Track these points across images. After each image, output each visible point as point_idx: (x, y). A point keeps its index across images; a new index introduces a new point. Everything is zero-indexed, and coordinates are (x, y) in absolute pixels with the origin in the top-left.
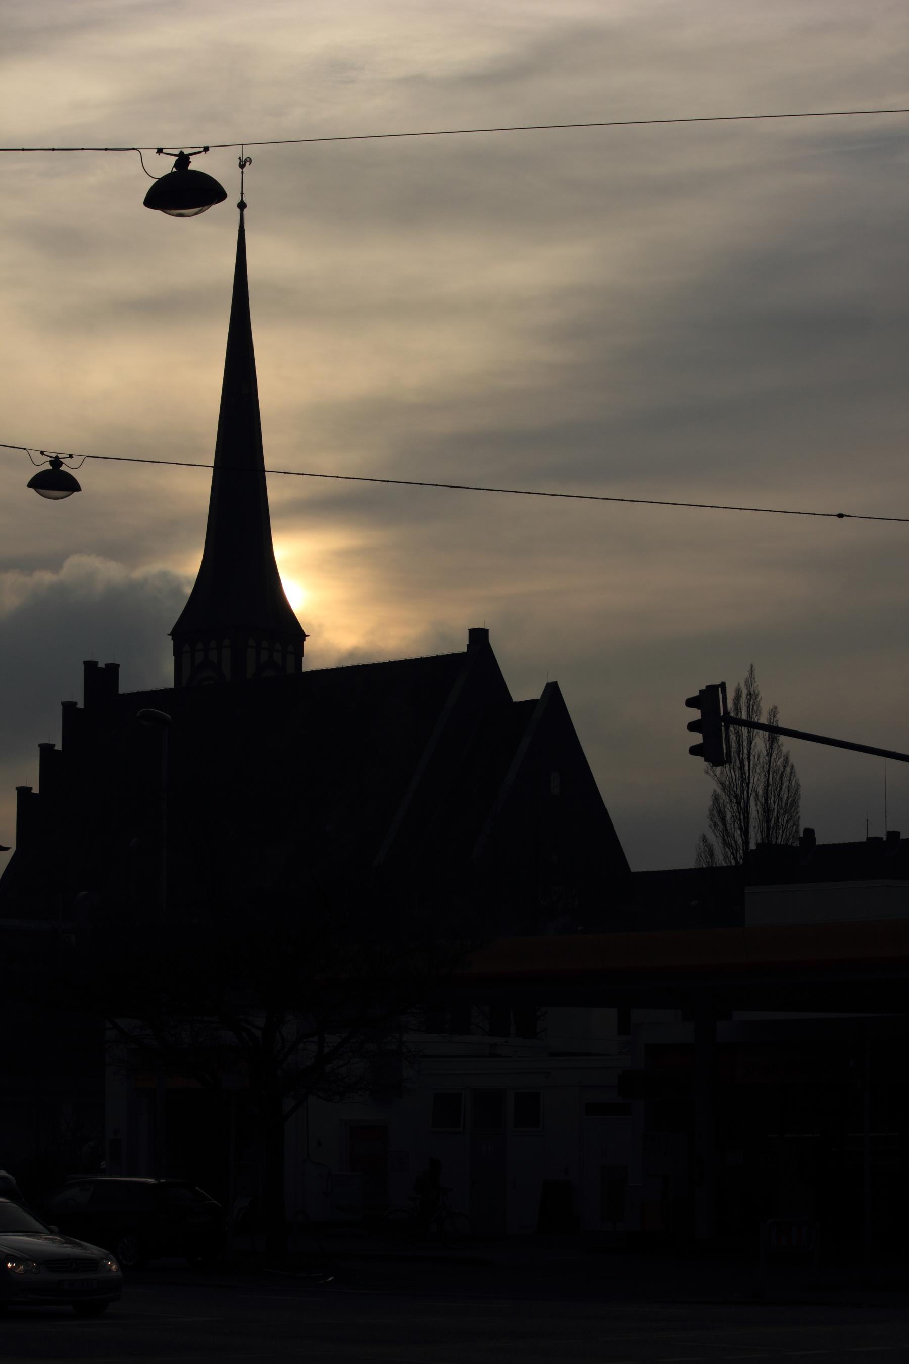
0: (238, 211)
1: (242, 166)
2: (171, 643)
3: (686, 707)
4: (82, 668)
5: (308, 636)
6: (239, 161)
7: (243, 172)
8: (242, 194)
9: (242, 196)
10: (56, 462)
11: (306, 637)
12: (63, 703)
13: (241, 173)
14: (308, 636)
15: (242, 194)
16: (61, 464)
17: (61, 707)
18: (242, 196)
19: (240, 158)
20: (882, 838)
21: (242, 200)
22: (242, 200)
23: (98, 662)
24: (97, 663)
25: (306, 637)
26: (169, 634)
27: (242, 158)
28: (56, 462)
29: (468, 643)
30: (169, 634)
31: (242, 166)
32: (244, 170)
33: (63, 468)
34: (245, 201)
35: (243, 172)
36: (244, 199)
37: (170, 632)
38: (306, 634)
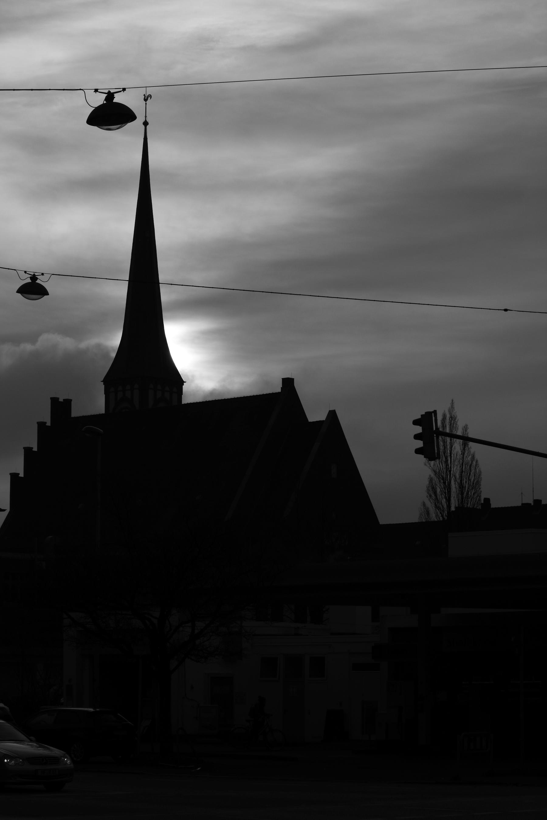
0: (143, 127)
2: (103, 387)
5: (185, 382)
7: (146, 104)
8: (146, 116)
9: (146, 118)
11: (184, 383)
14: (185, 382)
15: (146, 116)
18: (146, 118)
20: (531, 504)
25: (184, 383)
34: (147, 121)
35: (146, 104)
37: (102, 380)
38: (184, 381)
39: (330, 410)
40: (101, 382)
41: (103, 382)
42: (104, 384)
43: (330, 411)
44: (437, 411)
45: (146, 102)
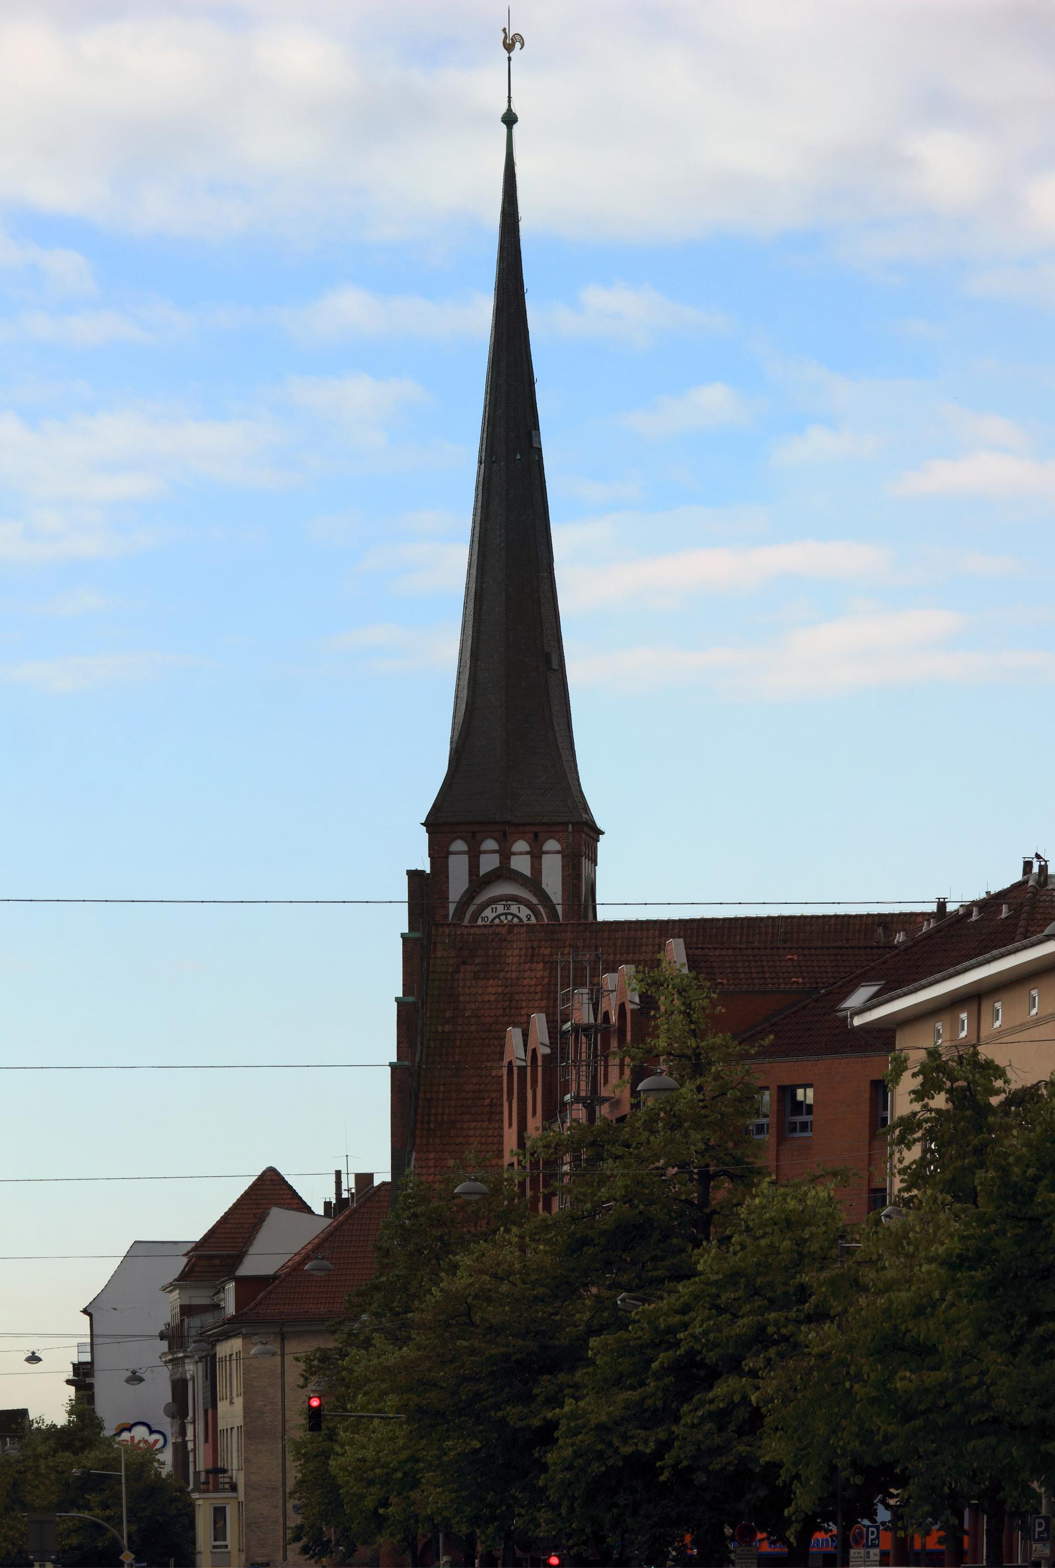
1: (509, 47)
4: (405, 880)
6: (503, 35)
7: (509, 59)
8: (509, 97)
9: (509, 102)
10: (33, 1353)
14: (422, 824)
16: (136, 1372)
18: (509, 102)
19: (504, 30)
20: (424, 871)
21: (509, 109)
22: (509, 109)
23: (27, 1409)
24: (364, 1180)
27: (507, 31)
28: (33, 1353)
31: (509, 47)
32: (511, 55)
33: (137, 1374)
35: (509, 59)
36: (512, 107)
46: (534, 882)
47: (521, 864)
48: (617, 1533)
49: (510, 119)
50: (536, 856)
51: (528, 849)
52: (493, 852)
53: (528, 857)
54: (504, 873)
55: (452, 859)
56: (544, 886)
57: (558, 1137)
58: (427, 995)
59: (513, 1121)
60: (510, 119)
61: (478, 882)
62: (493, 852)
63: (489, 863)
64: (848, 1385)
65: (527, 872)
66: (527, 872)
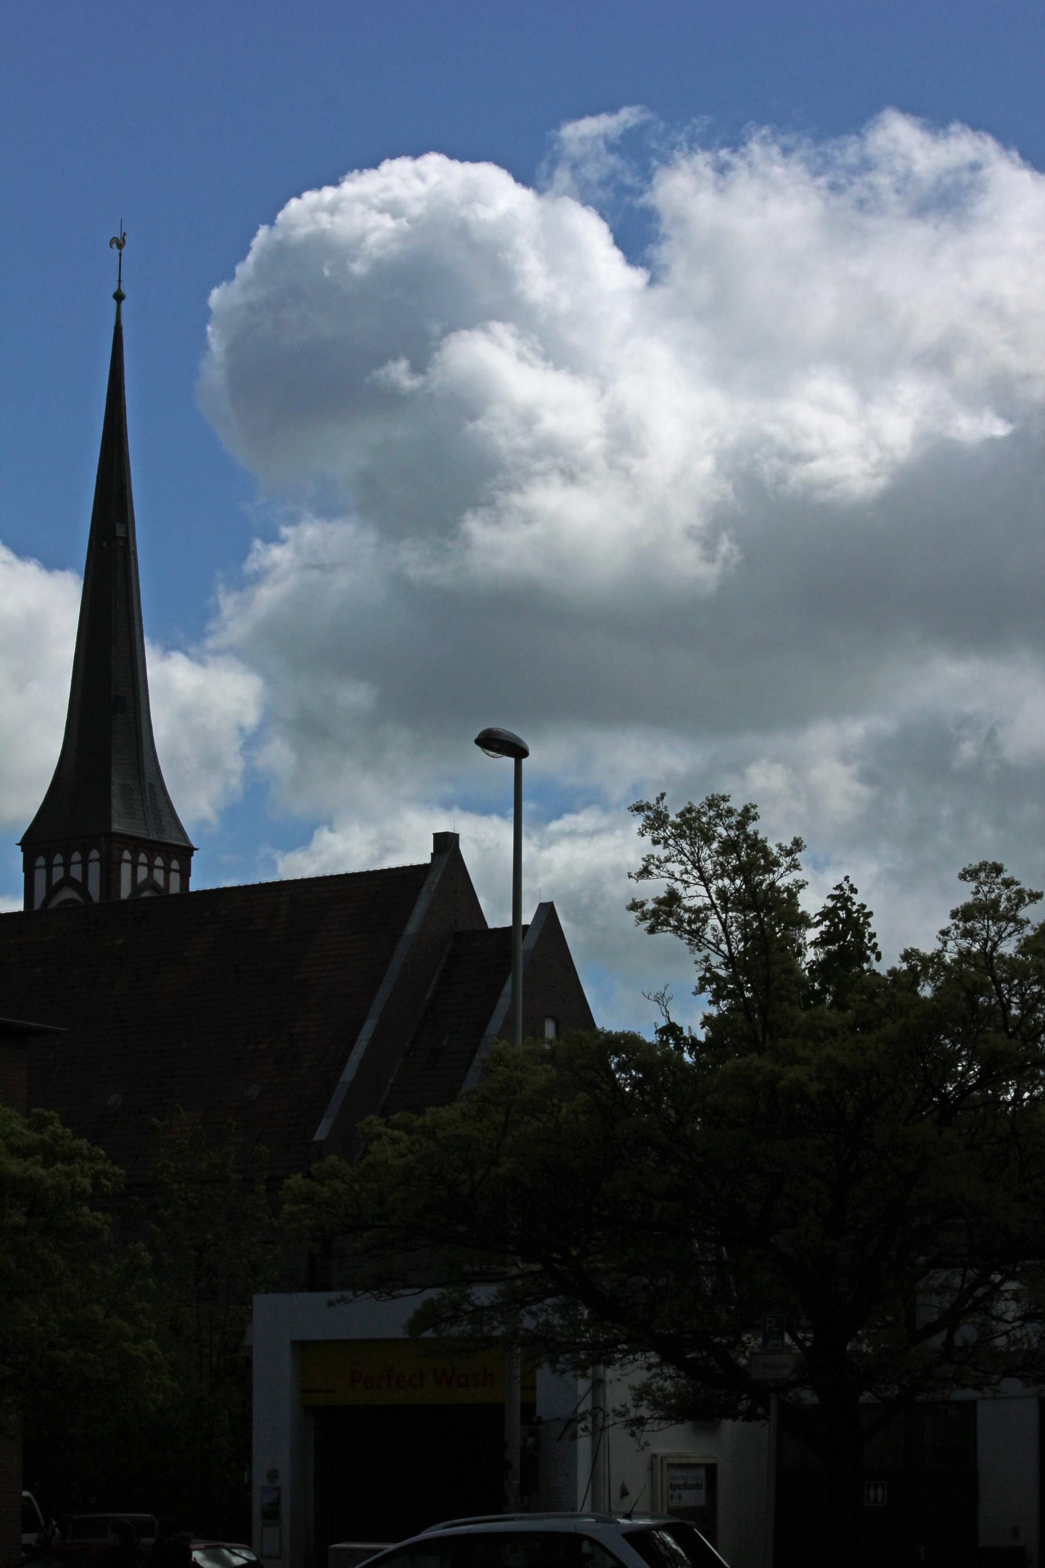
0: (114, 302)
2: (20, 855)
3: (474, 744)
5: (197, 849)
7: (120, 254)
8: (120, 281)
9: (120, 284)
11: (195, 852)
12: (434, 834)
13: (118, 254)
14: (197, 849)
15: (120, 281)
17: (433, 836)
18: (120, 284)
20: (655, 907)
21: (119, 290)
22: (119, 290)
25: (195, 852)
26: (18, 844)
29: (432, 852)
30: (18, 844)
34: (123, 291)
35: (120, 254)
36: (122, 288)
37: (19, 842)
38: (195, 847)
39: (541, 902)
40: (666, 886)
41: (20, 847)
42: (22, 851)
43: (541, 905)
44: (460, 836)
45: (121, 250)
46: (82, 887)
47: (76, 872)
48: (105, 1226)
49: (119, 297)
50: (85, 863)
51: (777, 884)
52: (77, 863)
53: (80, 866)
54: (68, 881)
55: (37, 871)
56: (89, 890)
57: (734, 940)
58: (615, 1424)
59: (36, 889)
60: (119, 297)
61: (52, 890)
62: (77, 863)
63: (58, 874)
64: (628, 1076)
65: (79, 878)
66: (79, 878)
